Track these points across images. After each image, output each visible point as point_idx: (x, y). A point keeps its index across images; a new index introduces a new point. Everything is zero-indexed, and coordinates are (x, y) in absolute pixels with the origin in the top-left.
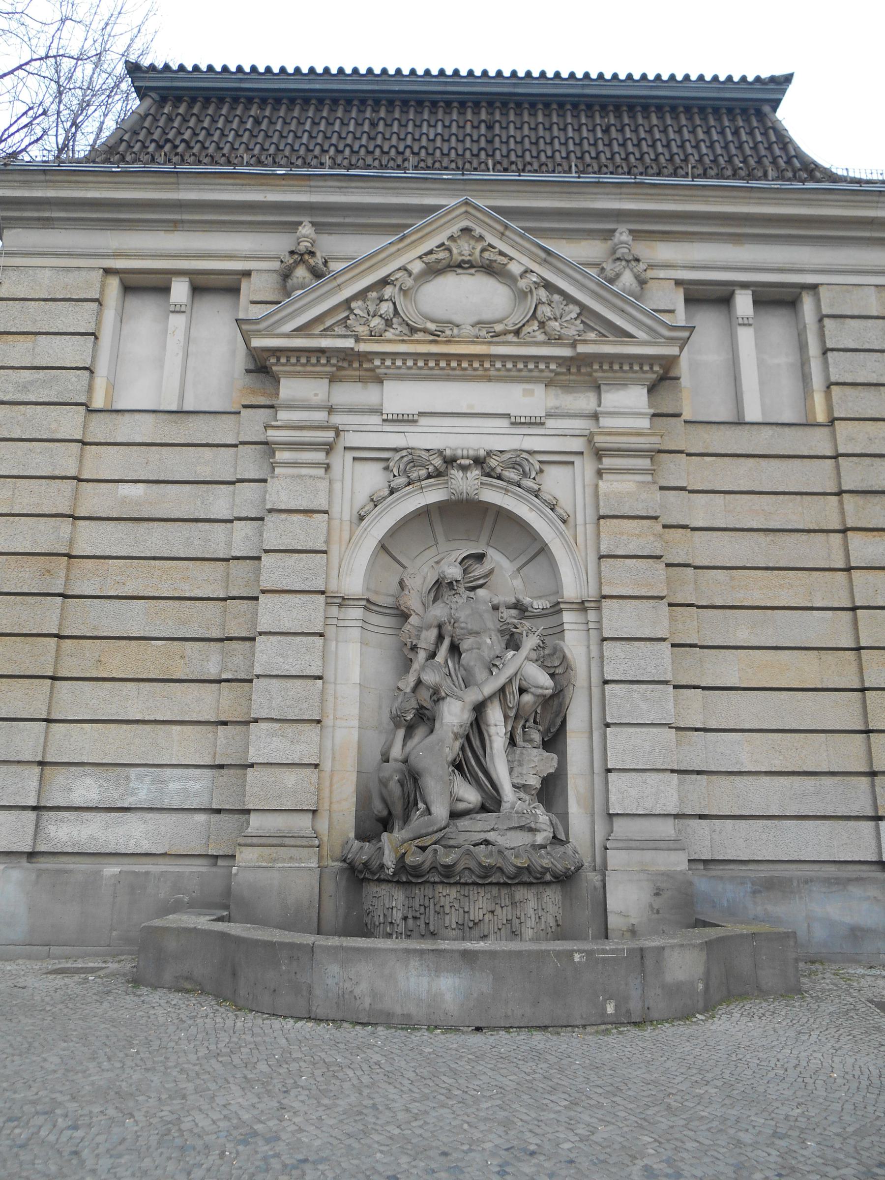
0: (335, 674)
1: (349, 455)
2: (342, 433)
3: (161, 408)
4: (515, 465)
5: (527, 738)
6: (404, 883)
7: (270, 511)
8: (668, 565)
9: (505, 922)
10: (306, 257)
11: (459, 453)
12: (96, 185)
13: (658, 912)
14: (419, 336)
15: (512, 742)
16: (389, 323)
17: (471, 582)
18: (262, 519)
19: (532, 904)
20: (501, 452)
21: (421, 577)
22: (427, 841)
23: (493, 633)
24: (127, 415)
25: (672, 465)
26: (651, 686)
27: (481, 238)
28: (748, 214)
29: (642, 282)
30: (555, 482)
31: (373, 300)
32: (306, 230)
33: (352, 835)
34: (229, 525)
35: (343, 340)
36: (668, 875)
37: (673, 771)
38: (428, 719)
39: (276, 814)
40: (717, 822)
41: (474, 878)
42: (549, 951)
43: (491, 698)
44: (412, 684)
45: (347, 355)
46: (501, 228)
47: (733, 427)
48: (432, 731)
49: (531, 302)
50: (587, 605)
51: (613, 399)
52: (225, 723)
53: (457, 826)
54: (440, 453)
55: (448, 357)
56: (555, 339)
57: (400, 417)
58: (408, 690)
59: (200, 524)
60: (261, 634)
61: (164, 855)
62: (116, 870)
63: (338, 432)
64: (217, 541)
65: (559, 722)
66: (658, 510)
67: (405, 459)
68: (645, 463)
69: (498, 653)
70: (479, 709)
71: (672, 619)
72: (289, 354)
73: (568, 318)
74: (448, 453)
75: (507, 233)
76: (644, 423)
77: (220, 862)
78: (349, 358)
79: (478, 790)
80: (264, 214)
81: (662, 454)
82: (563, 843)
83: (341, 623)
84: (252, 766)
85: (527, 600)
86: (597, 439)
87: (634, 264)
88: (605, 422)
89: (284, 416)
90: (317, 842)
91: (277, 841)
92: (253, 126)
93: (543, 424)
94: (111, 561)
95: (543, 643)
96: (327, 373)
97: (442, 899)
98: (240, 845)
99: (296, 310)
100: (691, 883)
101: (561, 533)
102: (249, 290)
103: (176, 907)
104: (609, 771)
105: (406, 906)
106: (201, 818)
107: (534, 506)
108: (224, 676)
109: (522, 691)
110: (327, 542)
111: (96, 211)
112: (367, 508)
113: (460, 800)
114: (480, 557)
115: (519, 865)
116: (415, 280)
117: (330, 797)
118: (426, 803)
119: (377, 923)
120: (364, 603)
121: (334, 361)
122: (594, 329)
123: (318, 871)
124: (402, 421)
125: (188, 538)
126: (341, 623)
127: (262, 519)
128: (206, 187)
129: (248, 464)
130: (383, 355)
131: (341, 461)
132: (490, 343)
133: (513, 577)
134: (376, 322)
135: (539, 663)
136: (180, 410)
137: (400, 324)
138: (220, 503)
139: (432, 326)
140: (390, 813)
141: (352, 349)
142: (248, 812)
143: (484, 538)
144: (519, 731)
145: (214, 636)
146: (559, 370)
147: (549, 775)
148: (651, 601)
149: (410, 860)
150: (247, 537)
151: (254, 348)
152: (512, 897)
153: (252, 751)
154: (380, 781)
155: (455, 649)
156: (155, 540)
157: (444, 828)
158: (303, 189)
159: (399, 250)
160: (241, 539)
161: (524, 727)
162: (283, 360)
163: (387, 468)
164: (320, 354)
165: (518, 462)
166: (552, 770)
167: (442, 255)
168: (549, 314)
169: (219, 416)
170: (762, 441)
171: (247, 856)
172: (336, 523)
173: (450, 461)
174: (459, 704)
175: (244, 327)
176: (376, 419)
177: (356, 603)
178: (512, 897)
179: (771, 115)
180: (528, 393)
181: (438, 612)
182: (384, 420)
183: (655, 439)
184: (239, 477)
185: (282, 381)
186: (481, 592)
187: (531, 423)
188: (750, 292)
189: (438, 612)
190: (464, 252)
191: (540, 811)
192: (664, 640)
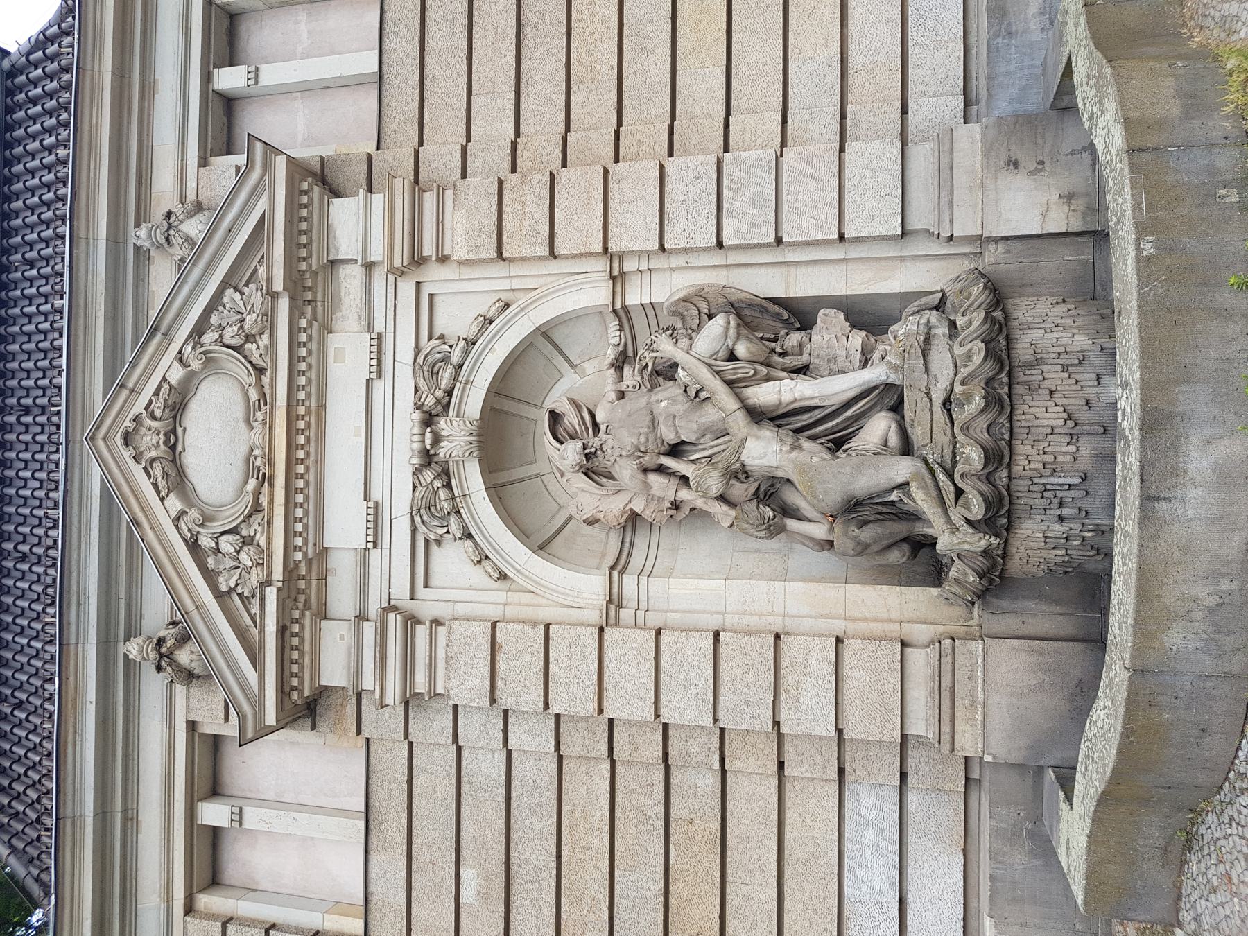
0: (712, 613)
1: (421, 591)
2: (392, 602)
3: (363, 841)
4: (433, 373)
5: (797, 350)
6: (1009, 522)
7: (493, 701)
8: (564, 165)
9: (1066, 375)
10: (164, 650)
11: (416, 446)
12: (75, 925)
13: (1042, 163)
14: (264, 500)
15: (803, 370)
16: (248, 541)
17: (587, 429)
18: (506, 712)
19: (1036, 335)
20: (416, 391)
21: (585, 498)
22: (949, 493)
23: (654, 398)
24: (372, 888)
25: (434, 165)
26: (726, 183)
27: (136, 419)
28: (113, 74)
29: (199, 207)
30: (455, 319)
31: (218, 562)
32: (133, 649)
33: (935, 591)
34: (514, 755)
35: (267, 602)
36: (987, 152)
37: (842, 149)
38: (772, 486)
39: (908, 698)
40: (912, 89)
41: (1003, 420)
42: (1139, 294)
43: (741, 399)
44: (725, 508)
45: (291, 593)
46: (125, 393)
47: (385, 86)
48: (788, 480)
49: (220, 352)
50: (616, 273)
51: (346, 243)
52: (781, 765)
53: (924, 446)
54: (417, 472)
55: (290, 462)
56: (269, 318)
57: (371, 525)
58: (733, 513)
59: (514, 794)
60: (657, 716)
61: (964, 851)
62: (988, 923)
63: (391, 608)
64: (535, 771)
65: (771, 306)
66: (491, 179)
67: (425, 518)
68: (429, 199)
69: (681, 391)
70: (757, 415)
71: (635, 157)
72: (287, 673)
73: (241, 303)
74: (416, 461)
75: (130, 385)
76: (378, 200)
77: (975, 774)
78: (293, 594)
79: (871, 417)
80: (115, 703)
81: (420, 178)
82: (943, 299)
83: (643, 605)
84: (839, 731)
85: (611, 354)
86: (397, 263)
87: (173, 218)
88: (377, 254)
89: (368, 682)
90: (948, 642)
91: (946, 696)
92: (24, 710)
93: (380, 336)
94: (564, 916)
95: (668, 329)
96: (313, 624)
97: (1032, 466)
98: (952, 750)
99: (229, 666)
100: (1000, 118)
101: (522, 309)
102: (212, 725)
103: (1043, 847)
104: (842, 238)
105: (1043, 517)
106: (913, 799)
107: (487, 345)
108: (717, 766)
109: (732, 357)
110: (533, 624)
111: (111, 923)
112: (490, 570)
113: (886, 441)
114: (555, 417)
115: (983, 354)
116: (191, 506)
117: (882, 621)
118: (892, 490)
119: (1067, 558)
120: (615, 573)
121: (296, 614)
122: (255, 270)
123: (988, 641)
124: (376, 521)
125: (532, 811)
126: (643, 605)
127: (506, 712)
128: (78, 780)
129: (432, 729)
130: (288, 548)
131: (427, 607)
132: (272, 407)
133: (583, 375)
134: (245, 559)
135: (694, 335)
136: (364, 815)
137: (250, 526)
138: (485, 766)
139: (252, 483)
140: (904, 540)
141: (279, 590)
142: (904, 737)
143: (531, 412)
144: (788, 361)
145: (662, 778)
146: (309, 316)
147: (847, 319)
148: (611, 186)
149: (977, 510)
150: (530, 731)
151: (278, 721)
152: (1028, 365)
153: (819, 731)
154: (859, 554)
155: (676, 450)
156: (534, 853)
157: (926, 463)
158: (80, 653)
159: (152, 528)
160: (532, 739)
161: (784, 354)
162: (295, 682)
163: (439, 543)
164: (288, 633)
165: (428, 368)
166: (841, 315)
167: (157, 471)
168: (235, 328)
169: (372, 767)
170: (402, 46)
171: (968, 742)
172: (510, 612)
173: (428, 458)
174: (751, 444)
175: (250, 735)
176: (374, 556)
177: (615, 586)
178: (1028, 365)
179: (13, 58)
180: (340, 357)
181: (626, 472)
182: (375, 547)
183: (398, 184)
184: (450, 741)
185: (323, 683)
186: (599, 418)
187: (379, 352)
188: (216, 70)
189: (626, 472)
190: (154, 441)
191: (900, 329)
192: (662, 167)
